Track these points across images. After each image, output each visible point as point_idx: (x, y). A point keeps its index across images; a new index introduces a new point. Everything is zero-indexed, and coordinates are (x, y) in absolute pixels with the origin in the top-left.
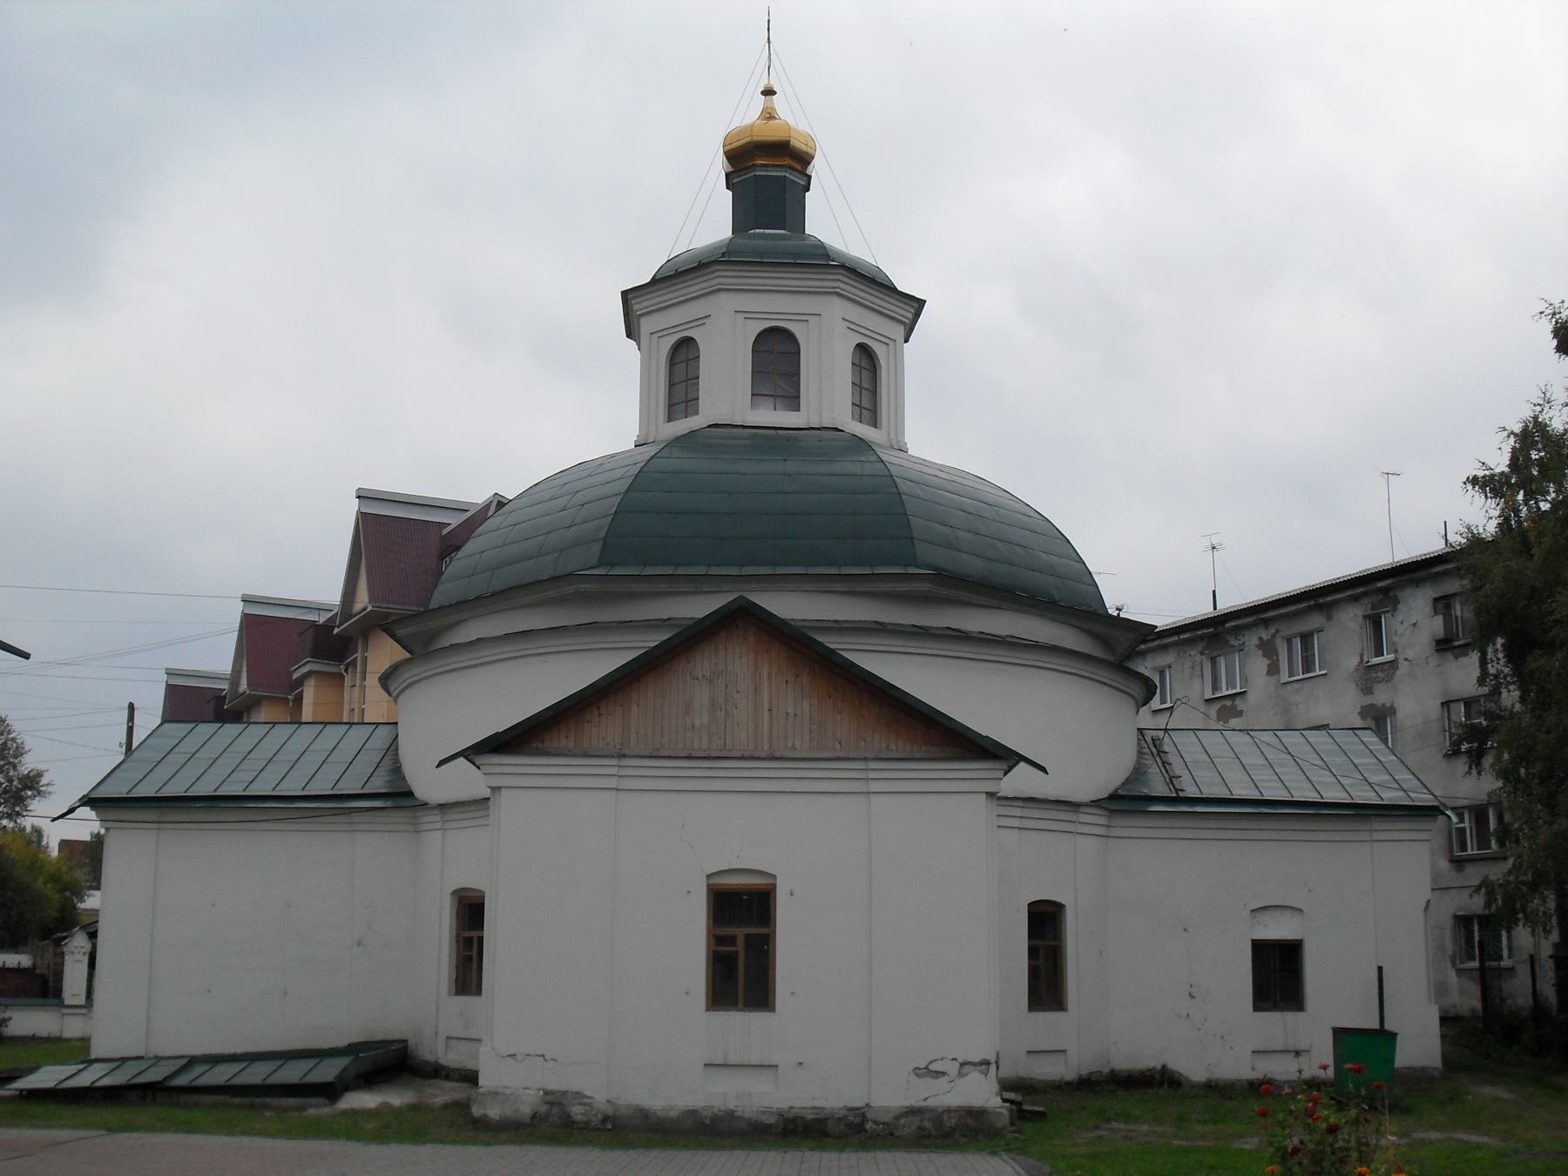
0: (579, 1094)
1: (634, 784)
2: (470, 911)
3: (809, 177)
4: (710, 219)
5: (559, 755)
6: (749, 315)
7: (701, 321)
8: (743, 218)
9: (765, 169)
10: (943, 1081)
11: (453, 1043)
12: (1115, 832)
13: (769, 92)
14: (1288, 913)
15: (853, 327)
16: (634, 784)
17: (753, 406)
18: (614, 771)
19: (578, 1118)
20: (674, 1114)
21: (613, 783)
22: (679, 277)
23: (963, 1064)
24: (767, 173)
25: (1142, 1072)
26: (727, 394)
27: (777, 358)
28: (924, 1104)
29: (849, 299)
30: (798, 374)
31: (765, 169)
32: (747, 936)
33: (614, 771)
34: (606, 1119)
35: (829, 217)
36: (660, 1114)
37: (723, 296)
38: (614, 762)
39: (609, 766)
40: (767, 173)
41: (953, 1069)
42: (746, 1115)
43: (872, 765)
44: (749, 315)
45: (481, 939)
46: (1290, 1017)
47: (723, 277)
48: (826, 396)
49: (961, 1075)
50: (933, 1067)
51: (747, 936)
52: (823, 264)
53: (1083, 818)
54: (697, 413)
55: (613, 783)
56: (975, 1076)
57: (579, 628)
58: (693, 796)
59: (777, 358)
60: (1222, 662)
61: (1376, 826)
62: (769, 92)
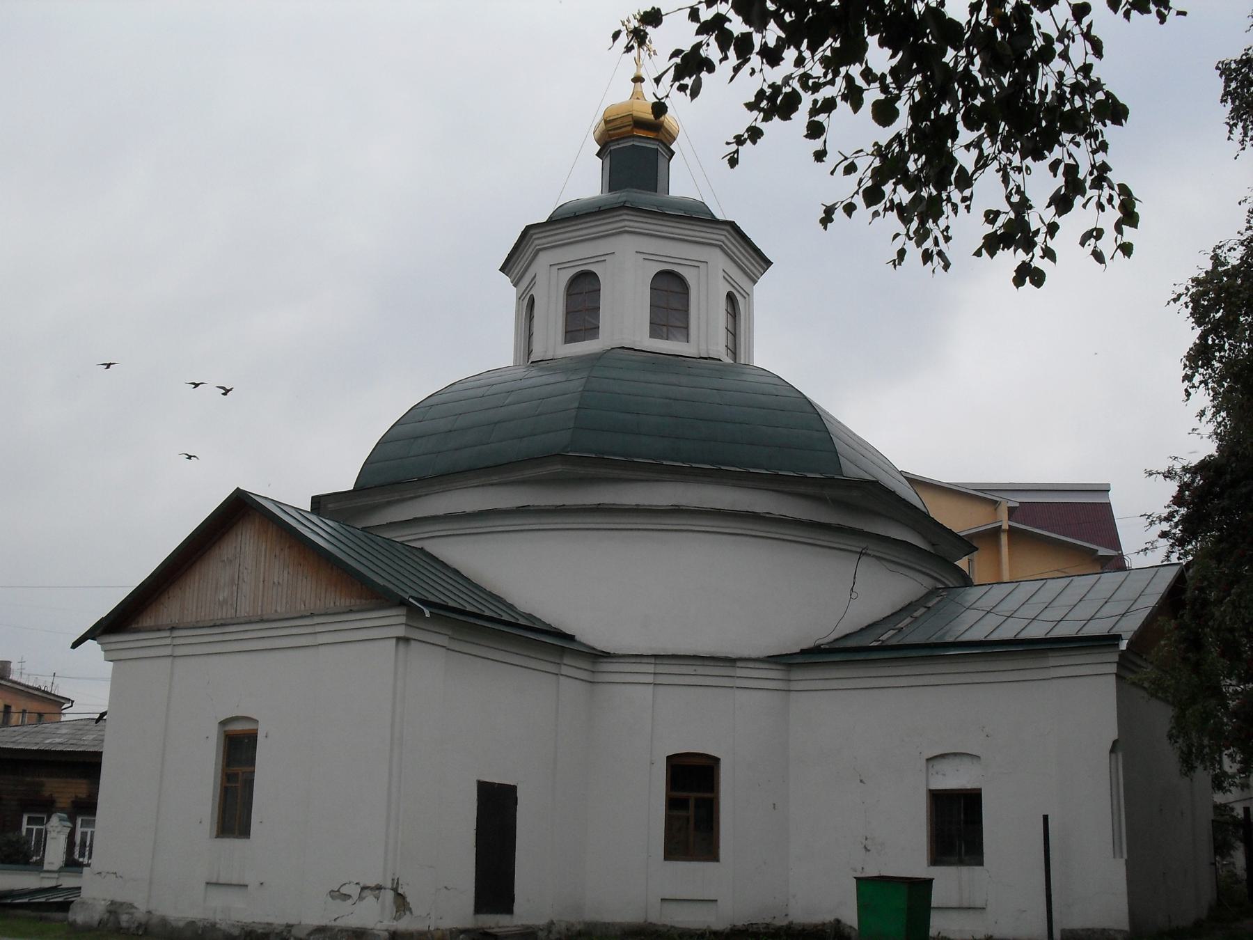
0: (131, 906)
1: (739, 683)
3: (673, 153)
4: (586, 180)
5: (159, 630)
6: (561, 266)
7: (696, 264)
8: (614, 180)
10: (350, 902)
12: (794, 686)
14: (966, 760)
15: (728, 278)
16: (739, 683)
18: (168, 641)
19: (124, 924)
20: (181, 924)
21: (168, 651)
22: (568, 218)
23: (363, 888)
25: (816, 926)
26: (626, 319)
27: (670, 293)
28: (333, 923)
32: (697, 800)
33: (168, 641)
34: (140, 926)
36: (174, 924)
37: (626, 237)
38: (167, 634)
39: (163, 638)
41: (354, 891)
42: (223, 926)
43: (317, 620)
44: (649, 257)
46: (965, 871)
48: (706, 335)
49: (361, 898)
50: (343, 890)
51: (697, 800)
53: (739, 672)
55: (168, 651)
56: (370, 899)
59: (670, 293)
61: (1052, 661)
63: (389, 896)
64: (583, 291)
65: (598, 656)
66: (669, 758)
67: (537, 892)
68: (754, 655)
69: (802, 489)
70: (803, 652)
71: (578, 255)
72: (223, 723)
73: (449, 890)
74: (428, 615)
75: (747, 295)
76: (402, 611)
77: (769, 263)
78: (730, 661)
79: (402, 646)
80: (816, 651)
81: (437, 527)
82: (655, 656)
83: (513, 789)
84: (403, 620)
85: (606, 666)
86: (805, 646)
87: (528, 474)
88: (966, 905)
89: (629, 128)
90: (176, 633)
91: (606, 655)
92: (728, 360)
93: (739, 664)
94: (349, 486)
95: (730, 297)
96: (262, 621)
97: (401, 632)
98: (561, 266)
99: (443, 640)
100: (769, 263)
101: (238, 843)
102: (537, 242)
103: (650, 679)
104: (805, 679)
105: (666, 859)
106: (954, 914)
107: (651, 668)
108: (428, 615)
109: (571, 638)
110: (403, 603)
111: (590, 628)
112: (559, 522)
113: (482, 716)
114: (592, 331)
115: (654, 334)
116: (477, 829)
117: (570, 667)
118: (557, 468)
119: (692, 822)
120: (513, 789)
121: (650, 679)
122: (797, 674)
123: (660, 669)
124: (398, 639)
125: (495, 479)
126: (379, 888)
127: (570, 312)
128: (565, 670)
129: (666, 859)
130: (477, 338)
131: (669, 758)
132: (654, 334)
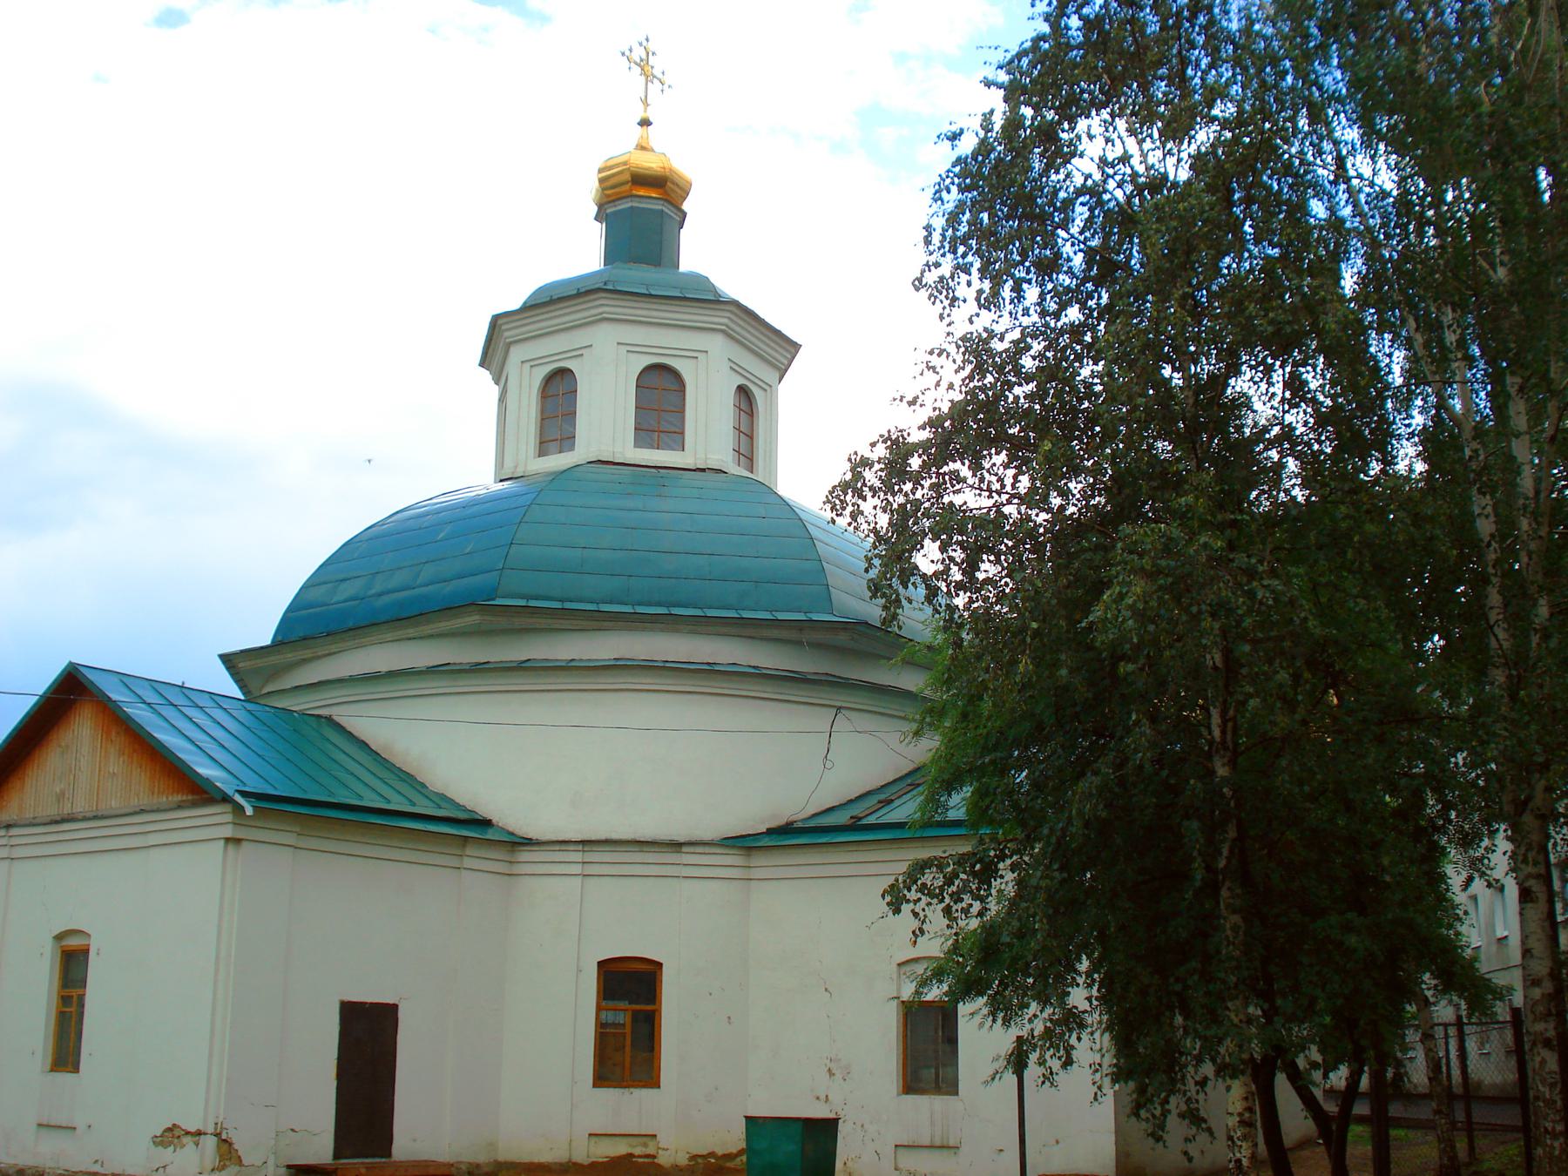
2: (73, 962)
3: (684, 215)
4: (581, 250)
6: (534, 363)
7: (693, 355)
8: (614, 252)
9: (649, 201)
11: (900, 1151)
13: (645, 123)
15: (735, 368)
17: (637, 445)
22: (552, 302)
24: (642, 209)
26: (606, 424)
27: (660, 394)
29: (737, 341)
30: (682, 411)
31: (649, 201)
32: (624, 1035)
35: (700, 251)
37: (605, 327)
40: (642, 209)
44: (634, 349)
45: (81, 998)
47: (608, 306)
48: (708, 436)
52: (702, 299)
54: (572, 448)
57: (478, 669)
58: (165, 851)
59: (660, 394)
60: (858, 754)
62: (645, 123)
63: (210, 1143)
64: (559, 388)
65: (518, 843)
66: (601, 964)
67: (413, 1132)
68: (707, 835)
69: (775, 633)
70: (770, 832)
71: (551, 349)
72: (59, 937)
73: (315, 1125)
74: (249, 811)
75: (769, 389)
76: (228, 808)
77: (794, 347)
78: (676, 846)
79: (231, 847)
80: (787, 830)
81: (336, 693)
82: (583, 842)
83: (394, 1008)
84: (229, 818)
85: (525, 855)
86: (774, 824)
87: (445, 625)
88: (938, 1143)
89: (627, 187)
90: (14, 831)
91: (528, 842)
92: (735, 469)
93: (685, 849)
94: (267, 641)
95: (743, 391)
96: (95, 818)
97: (228, 831)
98: (534, 363)
99: (290, 839)
100: (794, 347)
101: (68, 1077)
102: (507, 334)
103: (577, 869)
104: (765, 865)
105: (595, 1086)
106: (925, 1154)
107: (577, 857)
108: (249, 811)
109: (486, 823)
110: (225, 799)
111: (509, 807)
112: (465, 684)
113: (367, 924)
114: (566, 441)
115: (638, 443)
116: (339, 1059)
117: (474, 858)
118: (472, 619)
119: (628, 1042)
120: (394, 1008)
121: (577, 869)
122: (759, 860)
123: (589, 857)
124: (227, 840)
125: (411, 632)
126: (199, 1133)
127: (545, 419)
128: (467, 862)
129: (595, 1086)
130: (448, 445)
131: (601, 964)
132: (638, 443)
